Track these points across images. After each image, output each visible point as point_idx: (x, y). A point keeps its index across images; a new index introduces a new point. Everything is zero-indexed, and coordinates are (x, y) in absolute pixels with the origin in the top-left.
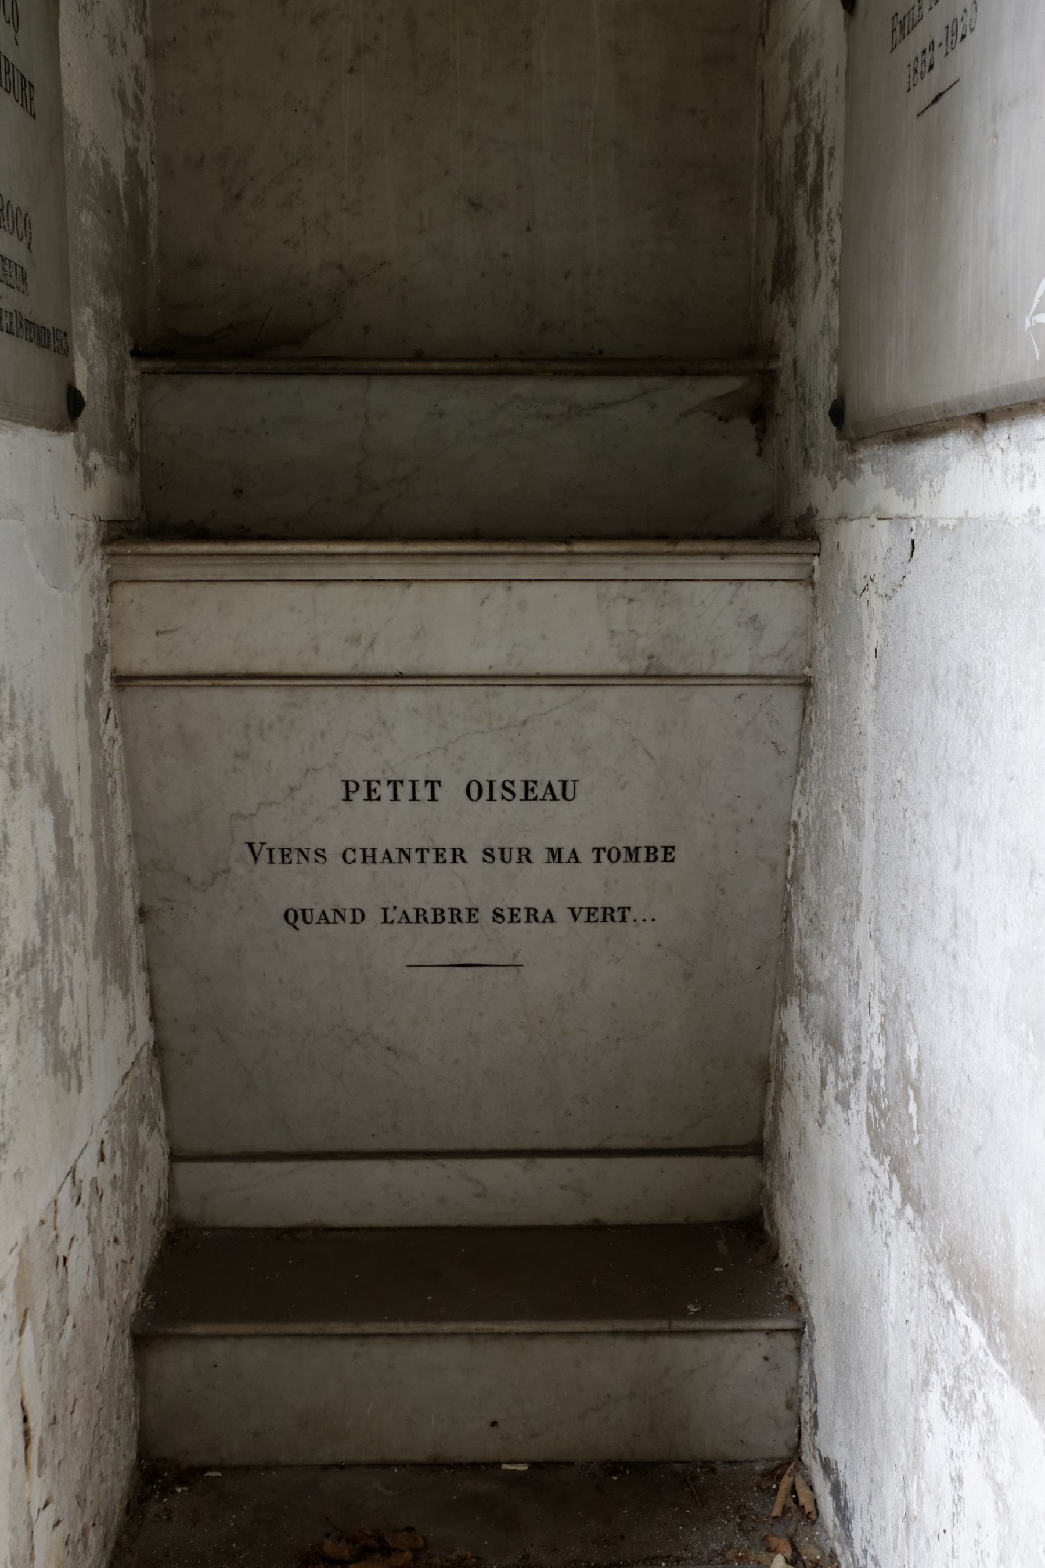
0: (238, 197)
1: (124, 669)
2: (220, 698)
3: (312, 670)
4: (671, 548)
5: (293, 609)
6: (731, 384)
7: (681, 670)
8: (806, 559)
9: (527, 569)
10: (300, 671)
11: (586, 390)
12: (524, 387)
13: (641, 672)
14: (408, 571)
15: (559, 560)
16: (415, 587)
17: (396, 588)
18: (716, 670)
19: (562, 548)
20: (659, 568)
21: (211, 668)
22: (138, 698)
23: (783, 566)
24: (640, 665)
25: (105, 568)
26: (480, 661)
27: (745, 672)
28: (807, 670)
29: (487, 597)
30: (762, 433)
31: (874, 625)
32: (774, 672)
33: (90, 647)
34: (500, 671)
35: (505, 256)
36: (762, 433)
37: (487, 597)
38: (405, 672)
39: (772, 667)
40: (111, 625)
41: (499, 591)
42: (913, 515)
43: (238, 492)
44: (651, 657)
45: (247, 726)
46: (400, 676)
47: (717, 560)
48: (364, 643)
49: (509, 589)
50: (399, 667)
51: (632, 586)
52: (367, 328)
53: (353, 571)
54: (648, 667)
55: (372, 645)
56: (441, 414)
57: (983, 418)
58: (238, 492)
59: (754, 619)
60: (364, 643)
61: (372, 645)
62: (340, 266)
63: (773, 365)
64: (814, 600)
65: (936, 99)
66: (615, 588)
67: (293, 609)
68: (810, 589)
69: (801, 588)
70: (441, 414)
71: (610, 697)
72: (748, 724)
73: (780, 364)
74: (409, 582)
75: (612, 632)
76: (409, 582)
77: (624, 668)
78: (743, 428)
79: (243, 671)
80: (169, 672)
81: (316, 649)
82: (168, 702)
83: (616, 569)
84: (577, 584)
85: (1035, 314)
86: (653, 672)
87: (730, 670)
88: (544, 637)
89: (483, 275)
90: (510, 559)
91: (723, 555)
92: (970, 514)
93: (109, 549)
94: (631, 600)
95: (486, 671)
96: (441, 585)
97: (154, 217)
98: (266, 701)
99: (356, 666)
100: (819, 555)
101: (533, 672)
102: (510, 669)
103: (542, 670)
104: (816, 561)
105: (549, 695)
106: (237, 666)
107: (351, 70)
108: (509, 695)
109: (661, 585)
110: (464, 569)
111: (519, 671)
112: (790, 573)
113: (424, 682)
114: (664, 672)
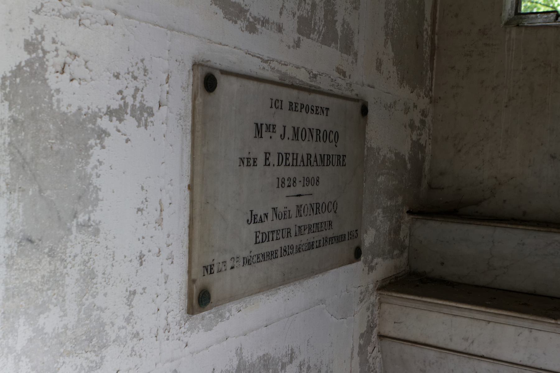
0: (460, 151)
1: (382, 333)
2: (415, 350)
3: (449, 347)
5: (443, 323)
9: (538, 326)
10: (444, 346)
14: (488, 318)
16: (491, 324)
17: (484, 323)
19: (553, 321)
21: (412, 339)
22: (387, 342)
25: (378, 298)
26: (516, 358)
29: (521, 333)
33: (364, 329)
34: (525, 363)
37: (521, 333)
38: (485, 355)
40: (379, 317)
41: (526, 332)
43: (442, 264)
45: (425, 361)
48: (470, 341)
49: (531, 332)
50: (482, 353)
52: (505, 201)
53: (467, 314)
55: (473, 342)
56: (523, 244)
58: (442, 264)
61: (473, 342)
62: (496, 178)
67: (443, 323)
70: (523, 244)
76: (489, 322)
79: (423, 342)
80: (398, 337)
81: (451, 340)
82: (397, 347)
88: (544, 354)
89: (554, 184)
93: (379, 292)
95: (518, 362)
96: (502, 325)
97: (428, 158)
98: (432, 354)
99: (466, 349)
101: (539, 367)
102: (529, 364)
103: (543, 367)
106: (421, 340)
107: (506, 106)
110: (511, 321)
111: (532, 365)
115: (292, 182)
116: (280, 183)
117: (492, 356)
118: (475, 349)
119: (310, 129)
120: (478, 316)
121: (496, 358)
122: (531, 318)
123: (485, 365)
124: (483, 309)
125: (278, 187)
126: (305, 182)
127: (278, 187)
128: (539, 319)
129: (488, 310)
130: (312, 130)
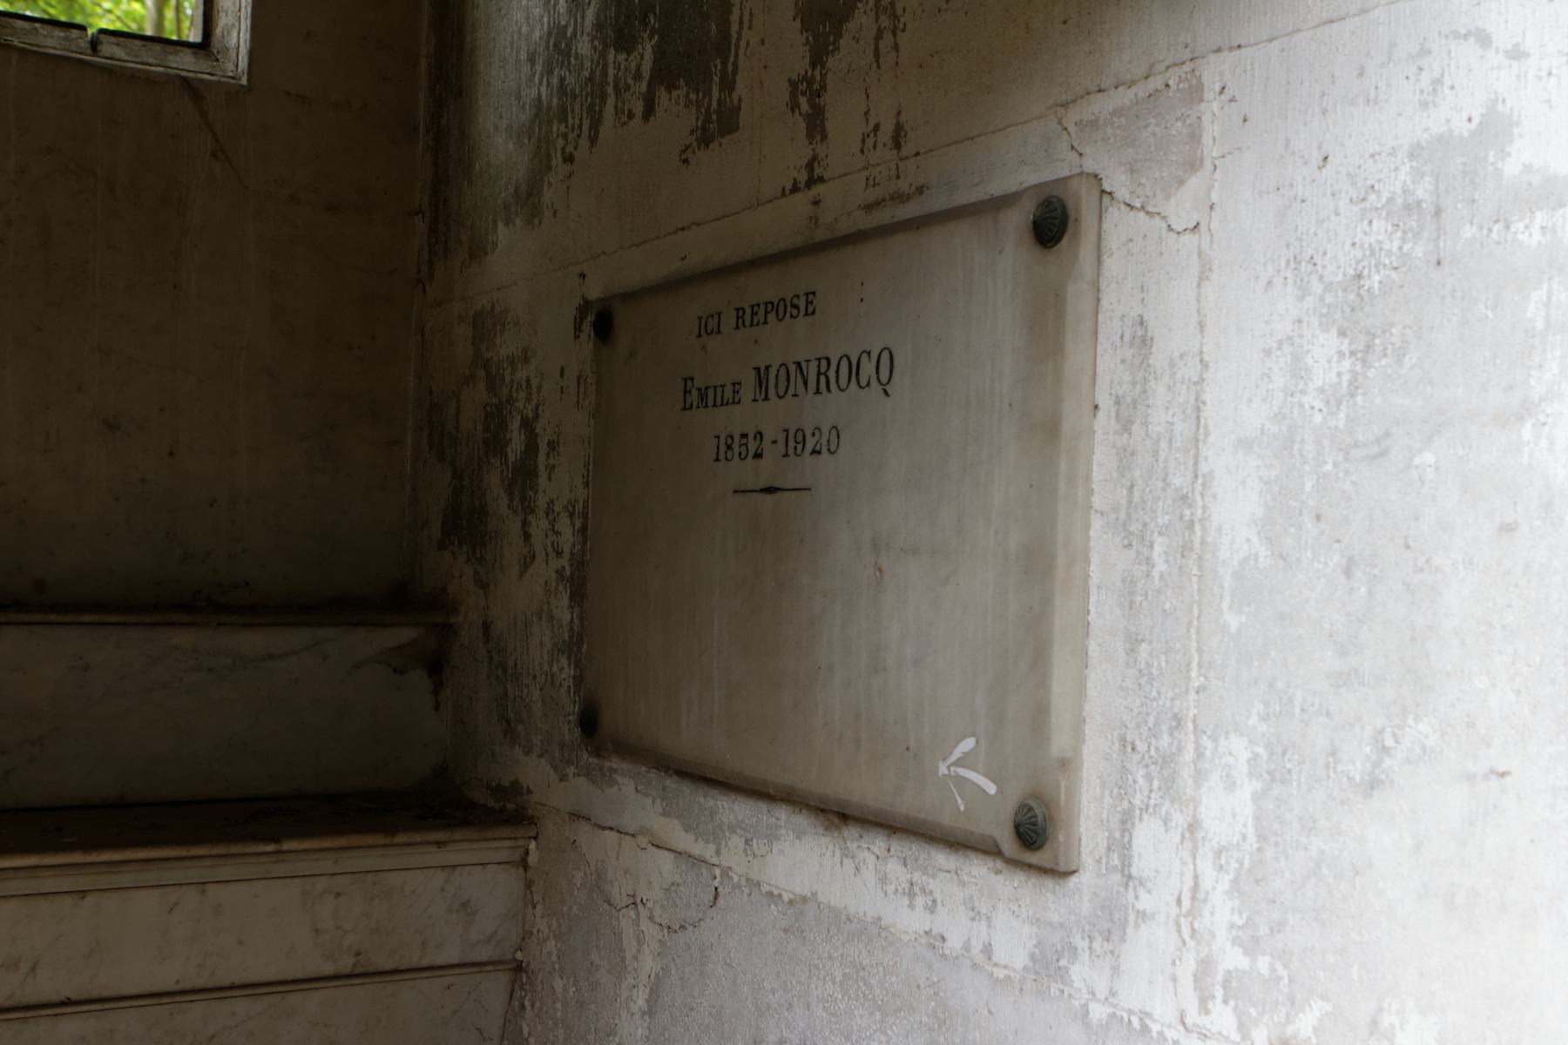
4: (388, 841)
6: (406, 634)
7: (389, 966)
8: (521, 843)
11: (251, 641)
12: (184, 638)
13: (347, 971)
15: (263, 859)
16: (91, 900)
18: (425, 963)
19: (271, 848)
20: (370, 861)
23: (499, 847)
24: (346, 964)
26: (165, 978)
27: (456, 961)
28: (519, 955)
30: (438, 687)
31: (646, 949)
32: (485, 958)
34: (187, 985)
35: (144, 480)
36: (438, 687)
38: (74, 997)
39: (482, 954)
42: (714, 861)
44: (358, 954)
46: (68, 1002)
47: (433, 849)
48: (24, 967)
49: (203, 892)
50: (67, 991)
51: (339, 879)
54: (354, 966)
55: (33, 969)
57: (839, 815)
59: (465, 904)
60: (24, 967)
61: (33, 969)
63: (453, 620)
64: (528, 885)
65: (770, 490)
66: (322, 883)
68: (521, 870)
69: (513, 870)
71: (312, 1001)
72: (455, 1012)
73: (460, 619)
74: (83, 893)
75: (317, 930)
76: (83, 893)
77: (328, 969)
78: (419, 679)
83: (327, 864)
84: (279, 882)
85: (957, 763)
86: (359, 970)
87: (440, 960)
90: (209, 862)
91: (439, 844)
92: (820, 898)
94: (338, 895)
95: (171, 987)
100: (535, 838)
101: (227, 983)
102: (200, 982)
103: (237, 980)
104: (533, 845)
105: (241, 1006)
108: (196, 1011)
109: (370, 877)
112: (504, 855)
113: (98, 1006)
114: (372, 969)
115: (736, 446)
116: (723, 448)
117: (95, 994)
118: (46, 987)
119: (799, 364)
120: (49, 883)
121: (106, 993)
122: (215, 851)
123: (72, 1026)
124: (77, 858)
125: (717, 460)
126: (792, 444)
127: (717, 460)
128: (236, 849)
129: (94, 857)
130: (804, 365)
